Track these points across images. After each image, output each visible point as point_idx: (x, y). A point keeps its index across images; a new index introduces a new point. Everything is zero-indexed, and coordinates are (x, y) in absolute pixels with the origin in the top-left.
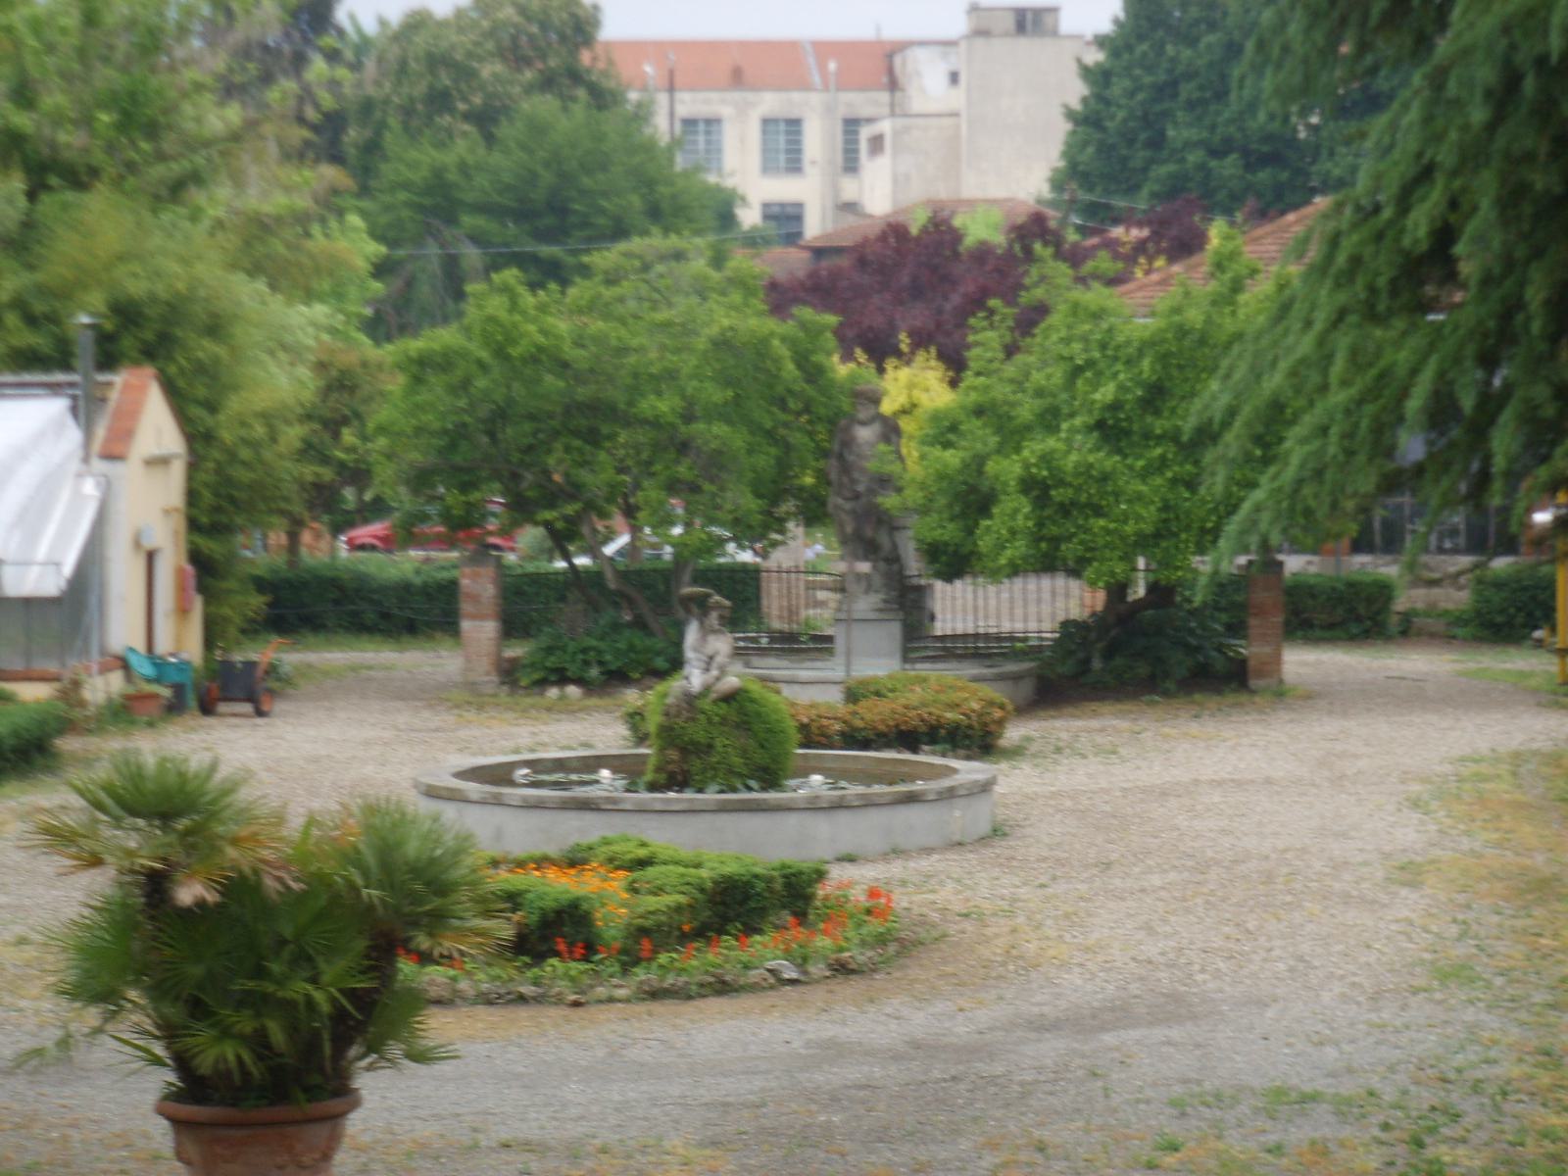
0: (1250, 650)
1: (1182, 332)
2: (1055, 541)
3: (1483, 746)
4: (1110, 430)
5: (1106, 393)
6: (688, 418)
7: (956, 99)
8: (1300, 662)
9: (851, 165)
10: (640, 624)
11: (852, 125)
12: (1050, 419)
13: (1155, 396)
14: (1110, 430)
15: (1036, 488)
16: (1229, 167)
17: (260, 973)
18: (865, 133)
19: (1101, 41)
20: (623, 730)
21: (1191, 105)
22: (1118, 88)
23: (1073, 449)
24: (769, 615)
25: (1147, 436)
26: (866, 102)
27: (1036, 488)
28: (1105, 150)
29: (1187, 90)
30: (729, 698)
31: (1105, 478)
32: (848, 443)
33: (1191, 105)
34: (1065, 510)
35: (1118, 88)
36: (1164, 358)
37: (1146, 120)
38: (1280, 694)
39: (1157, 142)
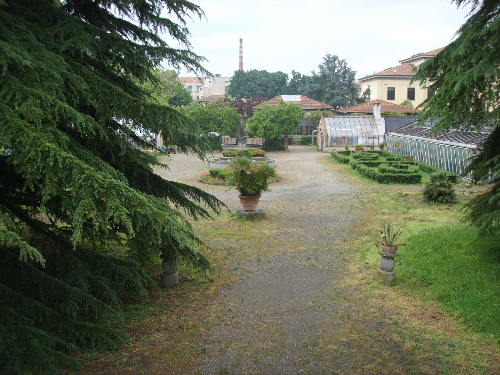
0: (285, 146)
1: (280, 110)
2: (266, 133)
3: (320, 156)
4: (272, 121)
5: (272, 117)
6: (223, 119)
7: (210, 84)
8: (290, 147)
9: (198, 92)
10: (216, 143)
11: (198, 87)
12: (264, 120)
13: (277, 117)
14: (272, 121)
15: (264, 128)
16: (247, 92)
17: (254, 181)
18: (200, 88)
19: (232, 78)
20: (222, 155)
21: (242, 85)
22: (234, 83)
23: (268, 123)
24: (88, 151)
25: (276, 121)
26: (200, 85)
27: (264, 128)
28: (233, 90)
29: (242, 83)
30: (245, 151)
31: (272, 126)
32: (240, 122)
33: (242, 85)
34: (268, 130)
35: (234, 83)
36: (278, 113)
37: (237, 87)
38: (289, 151)
39: (239, 89)
